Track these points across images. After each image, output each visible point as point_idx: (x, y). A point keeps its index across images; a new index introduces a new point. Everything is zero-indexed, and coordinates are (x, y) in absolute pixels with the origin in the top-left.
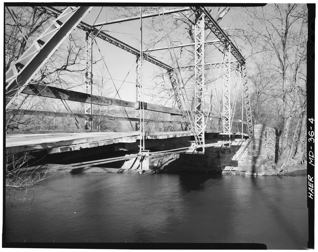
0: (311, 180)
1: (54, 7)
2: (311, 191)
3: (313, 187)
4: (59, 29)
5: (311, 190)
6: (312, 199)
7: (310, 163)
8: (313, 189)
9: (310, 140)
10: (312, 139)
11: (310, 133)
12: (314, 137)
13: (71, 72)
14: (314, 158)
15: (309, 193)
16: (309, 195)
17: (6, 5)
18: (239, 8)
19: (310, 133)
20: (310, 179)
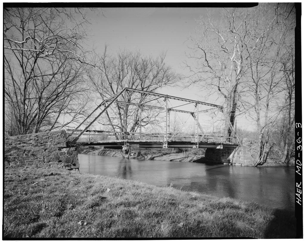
2: (299, 196)
6: (301, 204)
7: (297, 171)
12: (301, 144)
15: (297, 198)
16: (297, 200)
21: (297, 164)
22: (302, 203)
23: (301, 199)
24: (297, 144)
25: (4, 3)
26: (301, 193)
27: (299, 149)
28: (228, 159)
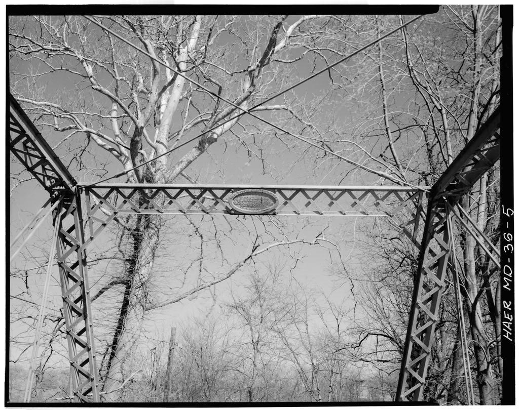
1: (24, 160)
2: (509, 327)
4: (499, 85)
5: (507, 324)
6: (511, 340)
7: (505, 287)
8: (511, 324)
9: (506, 248)
10: (510, 247)
12: (512, 242)
13: (400, 136)
14: (513, 278)
15: (504, 329)
16: (505, 333)
20: (506, 306)
21: (505, 273)
22: (513, 337)
23: (511, 330)
24: (504, 243)
25: (514, 404)
26: (511, 320)
27: (508, 249)
28: (434, 224)
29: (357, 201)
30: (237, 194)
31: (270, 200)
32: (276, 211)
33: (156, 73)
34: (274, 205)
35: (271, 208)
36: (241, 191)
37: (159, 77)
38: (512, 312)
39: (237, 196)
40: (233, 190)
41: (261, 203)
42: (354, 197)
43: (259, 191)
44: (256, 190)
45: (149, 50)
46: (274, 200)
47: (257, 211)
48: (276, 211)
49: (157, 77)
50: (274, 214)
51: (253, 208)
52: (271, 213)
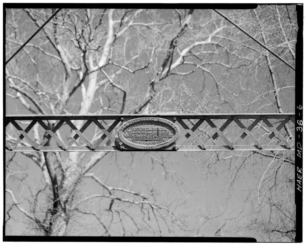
0: (300, 171)
2: (300, 183)
3: (301, 179)
9: (298, 129)
11: (299, 122)
14: (302, 151)
16: (298, 187)
17: (299, 8)
18: (6, 230)
19: (299, 122)
29: (247, 132)
30: (128, 124)
31: (168, 130)
32: (177, 146)
33: (68, 76)
34: (173, 137)
35: (170, 141)
36: (132, 120)
37: (70, 80)
38: (301, 175)
39: (128, 127)
40: (122, 118)
41: (158, 135)
42: (242, 126)
43: (155, 119)
44: (151, 119)
45: (61, 54)
46: (174, 131)
47: (153, 145)
48: (177, 146)
49: (68, 79)
50: (174, 150)
51: (148, 142)
52: (170, 148)
